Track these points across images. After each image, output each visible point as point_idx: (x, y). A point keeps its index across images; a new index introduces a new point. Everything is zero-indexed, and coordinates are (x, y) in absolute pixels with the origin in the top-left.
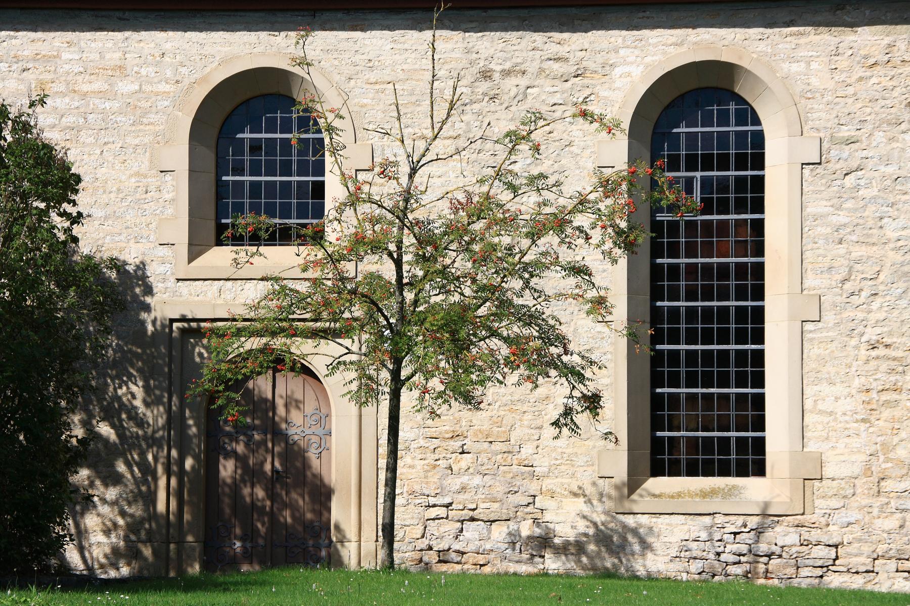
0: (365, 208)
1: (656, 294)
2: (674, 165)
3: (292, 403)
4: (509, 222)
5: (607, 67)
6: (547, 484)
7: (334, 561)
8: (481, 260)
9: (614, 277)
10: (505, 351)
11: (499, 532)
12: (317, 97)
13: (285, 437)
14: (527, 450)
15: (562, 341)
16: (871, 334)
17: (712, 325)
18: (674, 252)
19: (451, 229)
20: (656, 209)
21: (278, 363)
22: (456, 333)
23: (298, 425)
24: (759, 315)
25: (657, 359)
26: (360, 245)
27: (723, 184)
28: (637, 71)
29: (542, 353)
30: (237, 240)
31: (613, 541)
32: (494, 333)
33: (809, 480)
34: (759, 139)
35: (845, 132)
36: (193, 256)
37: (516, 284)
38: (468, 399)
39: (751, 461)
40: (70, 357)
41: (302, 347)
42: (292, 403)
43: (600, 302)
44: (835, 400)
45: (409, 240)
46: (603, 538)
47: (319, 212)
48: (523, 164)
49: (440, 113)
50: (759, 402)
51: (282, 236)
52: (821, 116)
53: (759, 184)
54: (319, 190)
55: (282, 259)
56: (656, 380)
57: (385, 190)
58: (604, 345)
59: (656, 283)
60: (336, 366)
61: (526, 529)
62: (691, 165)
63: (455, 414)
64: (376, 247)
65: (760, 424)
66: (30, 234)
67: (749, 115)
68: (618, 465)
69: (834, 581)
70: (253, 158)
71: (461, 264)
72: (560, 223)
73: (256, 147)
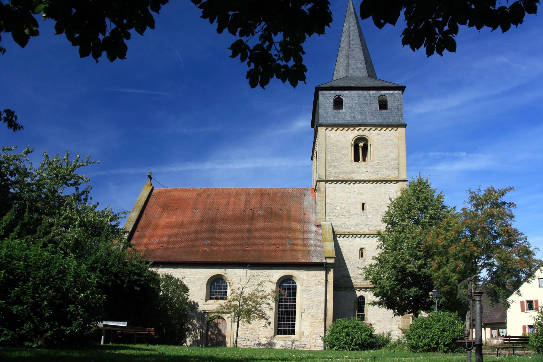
0: (234, 294)
1: (279, 308)
2: (283, 289)
3: (220, 323)
4: (258, 297)
5: (273, 275)
6: (261, 336)
7: (226, 346)
8: (254, 302)
9: (273, 305)
10: (256, 315)
11: (253, 343)
12: (227, 279)
13: (218, 328)
14: (258, 331)
15: (265, 314)
16: (312, 314)
17: (288, 313)
18: (282, 302)
19: (248, 298)
20: (280, 296)
21: (219, 317)
22: (248, 313)
23: (221, 326)
24: (295, 311)
25: (279, 317)
26: (234, 299)
27: (290, 293)
28: (277, 276)
29: (262, 316)
30: (213, 299)
31: (271, 344)
32: (255, 313)
33: (302, 335)
34: (296, 286)
35: (309, 285)
36: (206, 301)
37: (258, 306)
38: (249, 323)
39: (293, 333)
40: (186, 316)
41: (223, 315)
42: (220, 323)
43: (272, 308)
44: (306, 324)
45: (242, 299)
46: (269, 344)
47: (226, 295)
48: (260, 288)
49: (247, 281)
50: (295, 324)
51: (221, 299)
52: (305, 283)
53: (296, 293)
54: (226, 292)
55: (222, 302)
56: (279, 321)
57: (239, 292)
58: (271, 315)
59: (279, 306)
60: (228, 318)
61: (257, 342)
62: (285, 290)
63: (247, 325)
64: (236, 300)
65: (294, 327)
66: (507, 232)
67: (294, 283)
68: (272, 333)
69: (304, 349)
70: (217, 288)
71: (250, 303)
72: (265, 297)
73: (217, 286)
